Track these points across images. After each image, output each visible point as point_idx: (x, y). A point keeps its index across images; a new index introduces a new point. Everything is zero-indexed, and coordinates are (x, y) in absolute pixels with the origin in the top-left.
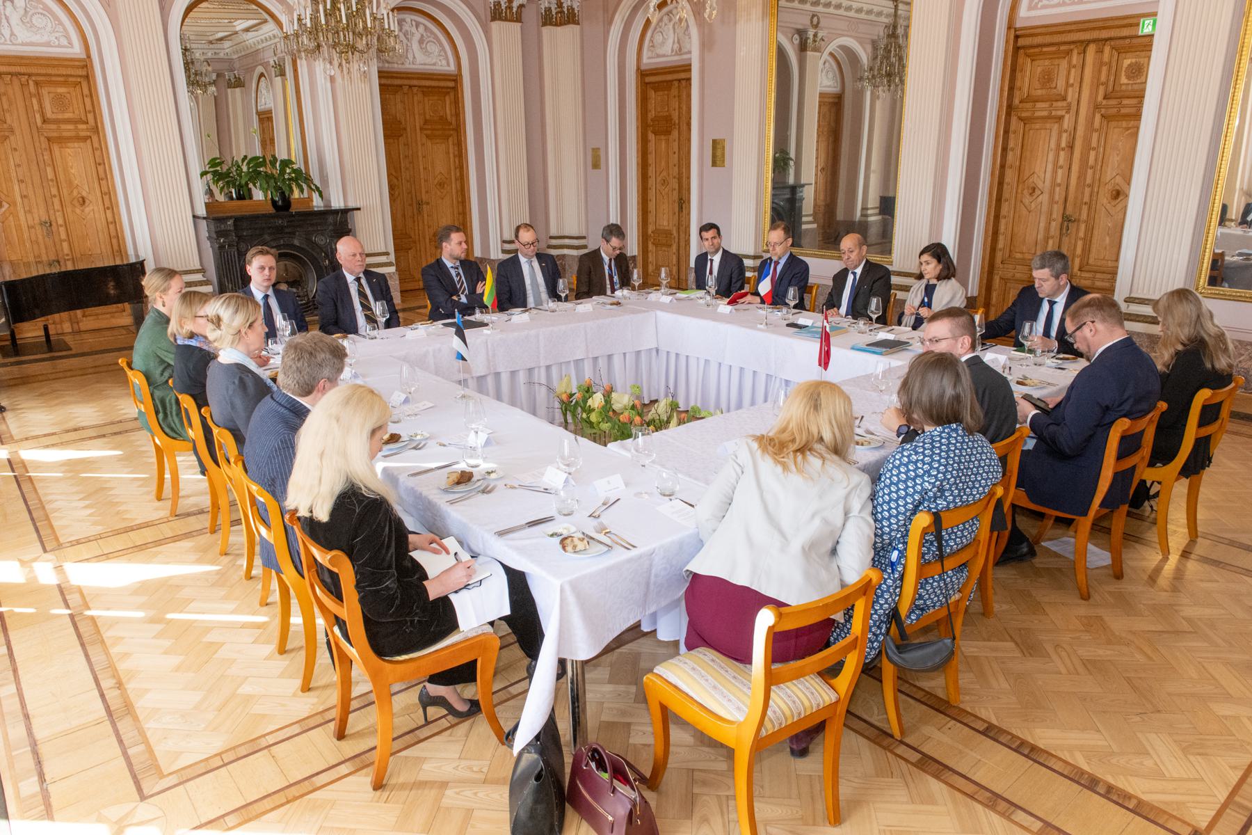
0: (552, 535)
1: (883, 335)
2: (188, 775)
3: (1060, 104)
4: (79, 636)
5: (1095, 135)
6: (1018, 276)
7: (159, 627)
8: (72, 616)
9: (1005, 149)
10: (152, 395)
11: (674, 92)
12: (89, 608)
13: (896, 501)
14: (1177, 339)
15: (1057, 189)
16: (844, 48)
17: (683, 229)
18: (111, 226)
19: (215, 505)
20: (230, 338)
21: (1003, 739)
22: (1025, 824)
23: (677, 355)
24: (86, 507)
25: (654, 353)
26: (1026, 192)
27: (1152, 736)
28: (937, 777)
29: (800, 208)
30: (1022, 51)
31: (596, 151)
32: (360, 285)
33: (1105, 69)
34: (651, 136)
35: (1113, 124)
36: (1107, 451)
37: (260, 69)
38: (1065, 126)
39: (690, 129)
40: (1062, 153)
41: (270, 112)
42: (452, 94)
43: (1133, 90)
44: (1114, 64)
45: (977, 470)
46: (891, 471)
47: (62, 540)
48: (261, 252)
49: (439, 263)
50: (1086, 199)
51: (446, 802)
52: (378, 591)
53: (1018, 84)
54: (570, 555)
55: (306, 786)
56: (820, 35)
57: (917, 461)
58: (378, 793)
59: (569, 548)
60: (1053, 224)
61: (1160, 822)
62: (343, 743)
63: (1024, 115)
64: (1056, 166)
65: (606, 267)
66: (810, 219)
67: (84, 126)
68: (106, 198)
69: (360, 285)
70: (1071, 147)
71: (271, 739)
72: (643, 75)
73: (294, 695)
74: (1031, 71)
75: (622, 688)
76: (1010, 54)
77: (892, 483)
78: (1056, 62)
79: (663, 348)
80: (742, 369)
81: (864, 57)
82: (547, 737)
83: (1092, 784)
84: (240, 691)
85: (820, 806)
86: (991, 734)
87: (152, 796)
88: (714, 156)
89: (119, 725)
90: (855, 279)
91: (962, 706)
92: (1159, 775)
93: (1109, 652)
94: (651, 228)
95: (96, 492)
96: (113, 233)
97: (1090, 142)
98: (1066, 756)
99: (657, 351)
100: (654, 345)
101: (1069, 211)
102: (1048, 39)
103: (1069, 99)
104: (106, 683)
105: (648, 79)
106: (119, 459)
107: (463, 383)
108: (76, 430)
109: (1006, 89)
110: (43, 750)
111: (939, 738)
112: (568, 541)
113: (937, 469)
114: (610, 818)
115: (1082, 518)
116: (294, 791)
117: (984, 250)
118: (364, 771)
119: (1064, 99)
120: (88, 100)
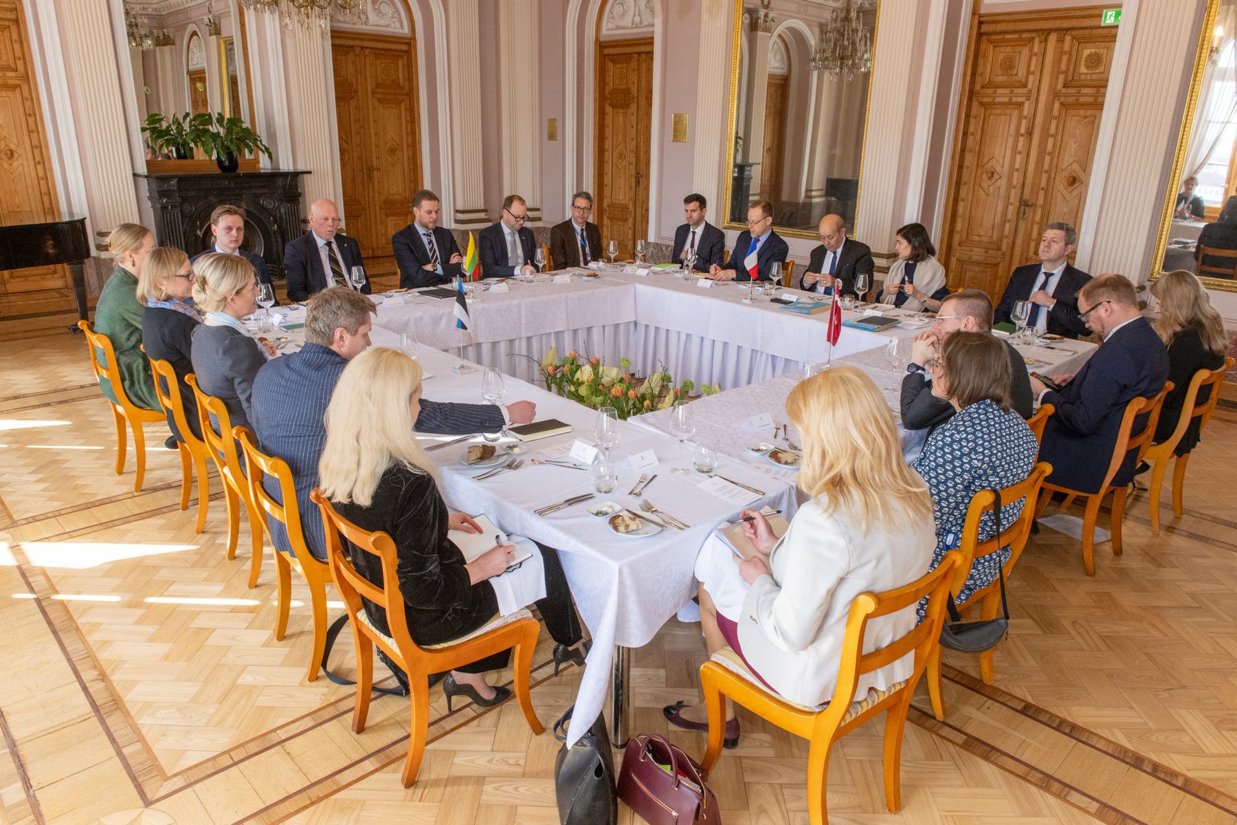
0: (597, 514)
1: (869, 312)
2: (197, 776)
3: (1020, 91)
4: (50, 623)
5: (1054, 123)
6: (975, 258)
7: (139, 612)
8: (38, 601)
9: (965, 134)
10: (118, 360)
11: (634, 65)
12: (57, 592)
13: (945, 483)
14: (1176, 320)
15: (1016, 174)
16: (795, 32)
17: (639, 204)
18: (42, 182)
19: (189, 480)
20: (215, 304)
21: (1044, 718)
22: (1083, 805)
23: (657, 328)
24: (38, 481)
25: (632, 326)
26: (984, 176)
27: (1183, 712)
28: (986, 758)
29: (748, 187)
30: (984, 38)
31: (552, 122)
32: (331, 249)
33: (1065, 58)
34: (608, 109)
35: (1073, 112)
36: (1121, 430)
37: (192, 27)
38: (1025, 113)
39: (650, 105)
40: (1021, 139)
41: (203, 71)
42: (405, 57)
43: (1092, 80)
44: (1074, 54)
45: (1009, 446)
46: (934, 453)
47: (15, 517)
48: (229, 212)
49: (411, 230)
50: (1043, 184)
51: (485, 798)
52: (422, 576)
53: (980, 70)
54: (622, 535)
55: (329, 786)
56: (771, 15)
57: (961, 439)
58: (411, 790)
59: (622, 528)
60: (1011, 208)
61: (1211, 799)
62: (363, 737)
63: (985, 100)
64: (1015, 152)
65: (579, 238)
66: (757, 198)
67: (13, 74)
68: (37, 152)
69: (331, 249)
70: (1030, 133)
71: (282, 734)
72: (602, 47)
73: (301, 685)
74: (993, 57)
75: (651, 672)
76: (974, 39)
77: (937, 465)
78: (1018, 49)
79: (642, 322)
80: (726, 344)
81: (812, 40)
82: (598, 732)
83: (1137, 762)
84: (240, 681)
85: (878, 795)
86: (1030, 713)
87: (157, 801)
88: (676, 130)
89: (109, 722)
90: (835, 258)
91: (996, 685)
92: (1198, 751)
93: (1125, 629)
94: (606, 202)
95: (47, 465)
96: (44, 190)
97: (1049, 128)
98: (1106, 733)
99: (636, 324)
100: (632, 319)
101: (1027, 195)
102: (1011, 27)
103: (1030, 86)
104: (88, 675)
105: (606, 51)
106: (69, 430)
107: (462, 352)
108: (16, 398)
109: (969, 73)
110: (24, 751)
111: (981, 718)
112: (619, 520)
113: (982, 445)
114: (674, 814)
115: (1091, 496)
116: (317, 792)
117: (943, 232)
118: (391, 767)
119: (1025, 86)
120: (17, 47)
